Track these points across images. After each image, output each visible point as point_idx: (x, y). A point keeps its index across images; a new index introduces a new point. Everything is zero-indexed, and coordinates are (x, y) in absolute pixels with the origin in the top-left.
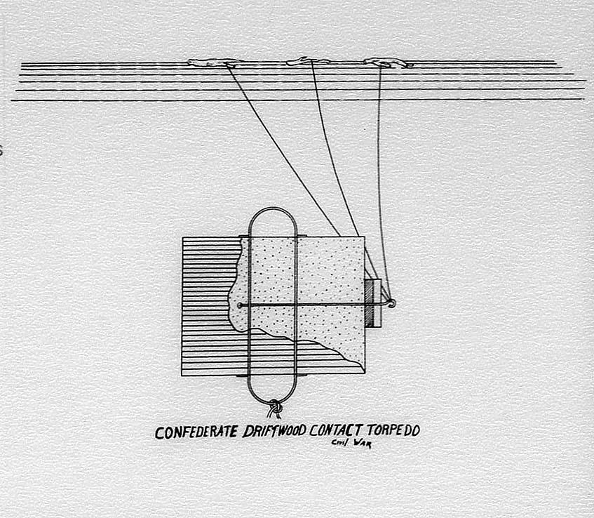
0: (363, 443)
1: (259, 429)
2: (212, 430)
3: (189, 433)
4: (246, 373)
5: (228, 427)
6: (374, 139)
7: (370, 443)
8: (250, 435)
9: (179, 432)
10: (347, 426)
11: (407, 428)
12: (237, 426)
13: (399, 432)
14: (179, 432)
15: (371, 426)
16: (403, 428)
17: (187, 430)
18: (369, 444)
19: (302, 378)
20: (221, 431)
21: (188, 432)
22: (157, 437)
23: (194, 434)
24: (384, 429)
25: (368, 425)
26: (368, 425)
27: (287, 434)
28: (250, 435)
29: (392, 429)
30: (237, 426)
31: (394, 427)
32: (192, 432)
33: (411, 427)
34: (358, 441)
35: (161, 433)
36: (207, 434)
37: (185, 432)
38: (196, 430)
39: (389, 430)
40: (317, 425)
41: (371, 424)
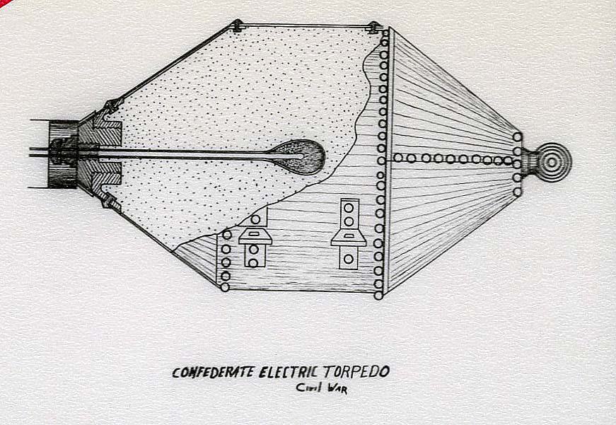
0: (339, 388)
2: (228, 371)
4: (510, 162)
5: (294, 368)
6: (169, 85)
8: (216, 376)
9: (193, 372)
10: (312, 368)
11: (212, 371)
14: (193, 372)
18: (344, 389)
22: (297, 388)
24: (344, 371)
27: (211, 377)
28: (216, 376)
34: (332, 385)
36: (222, 374)
39: (350, 373)
40: (179, 369)
41: (295, 366)
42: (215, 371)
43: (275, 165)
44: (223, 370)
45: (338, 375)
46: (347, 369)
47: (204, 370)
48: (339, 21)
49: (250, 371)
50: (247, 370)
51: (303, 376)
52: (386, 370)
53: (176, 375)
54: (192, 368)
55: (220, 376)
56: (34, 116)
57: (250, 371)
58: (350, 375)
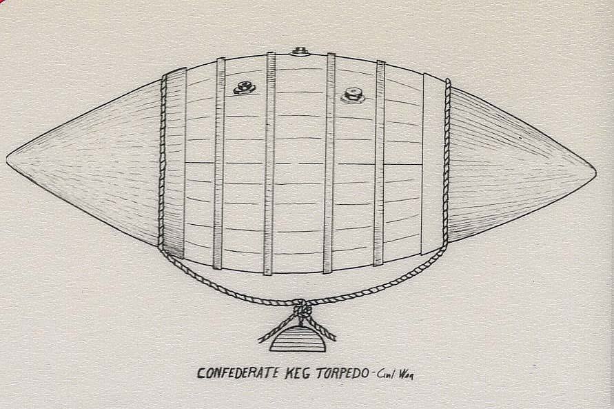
1: (336, 370)
3: (228, 374)
7: (412, 375)
9: (217, 372)
13: (231, 375)
14: (217, 372)
15: (321, 369)
17: (226, 371)
20: (260, 374)
23: (234, 375)
24: (334, 372)
31: (344, 370)
32: (231, 373)
33: (359, 370)
35: (203, 373)
37: (224, 372)
38: (234, 371)
44: (246, 370)
46: (336, 370)
47: (228, 371)
48: (400, 255)
49: (276, 372)
51: (261, 377)
53: (201, 375)
56: (299, 201)
57: (276, 372)
58: (339, 376)
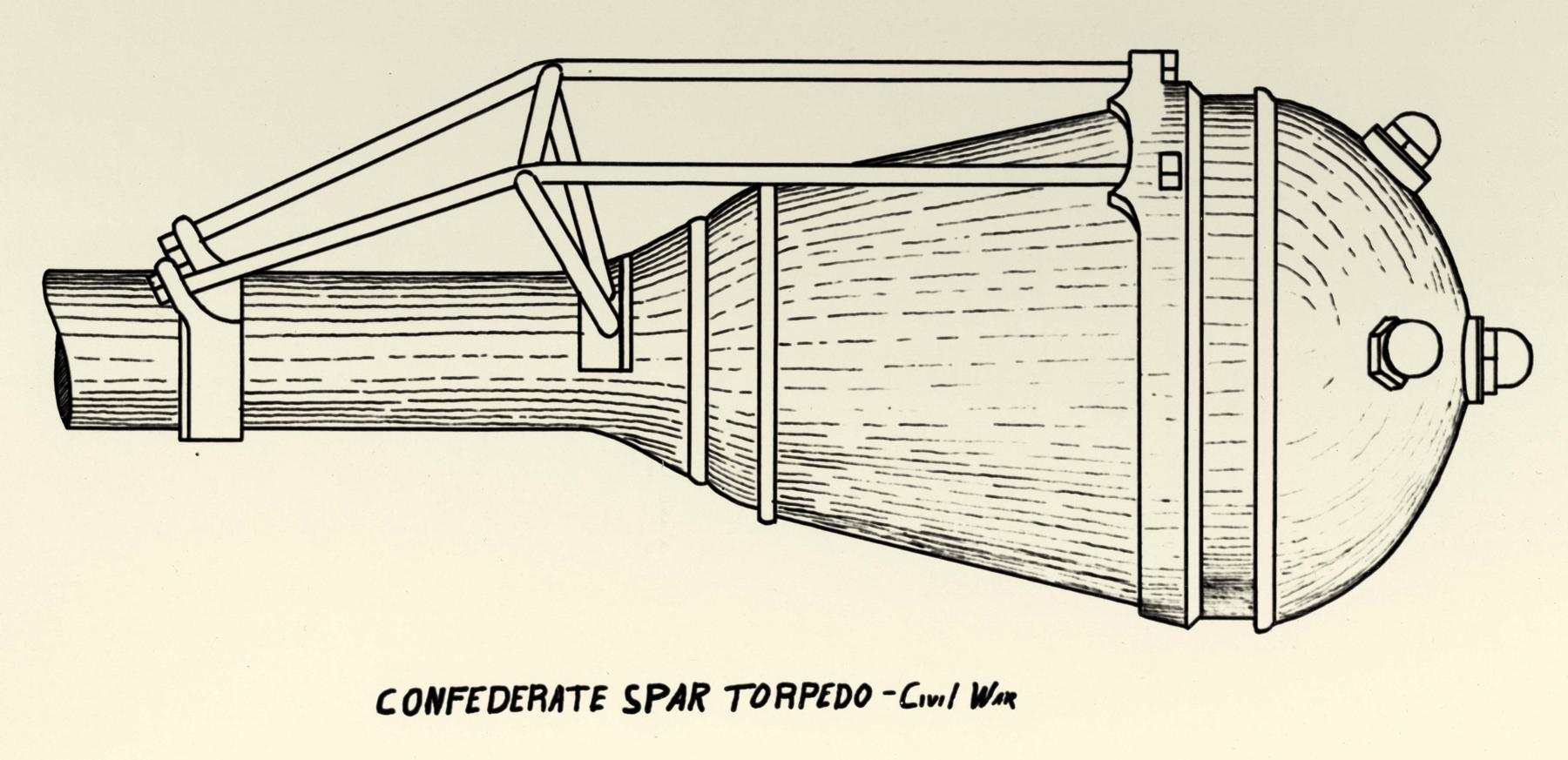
3: (465, 703)
5: (577, 689)
9: (436, 700)
12: (604, 688)
15: (736, 689)
16: (483, 698)
19: (638, 305)
20: (559, 698)
21: (461, 698)
25: (728, 689)
26: (728, 689)
29: (804, 695)
30: (604, 688)
31: (810, 690)
32: (472, 698)
40: (392, 691)
42: (844, 692)
43: (583, 334)
45: (416, 711)
50: (587, 697)
52: (864, 694)
54: (432, 690)
55: (515, 709)
